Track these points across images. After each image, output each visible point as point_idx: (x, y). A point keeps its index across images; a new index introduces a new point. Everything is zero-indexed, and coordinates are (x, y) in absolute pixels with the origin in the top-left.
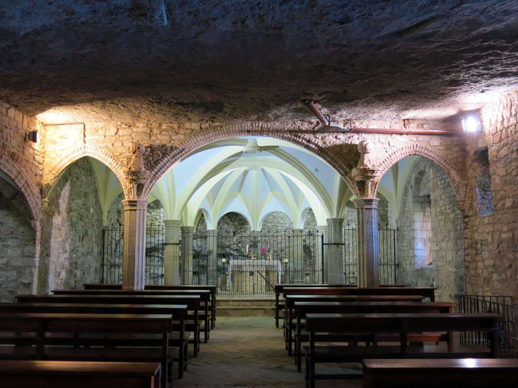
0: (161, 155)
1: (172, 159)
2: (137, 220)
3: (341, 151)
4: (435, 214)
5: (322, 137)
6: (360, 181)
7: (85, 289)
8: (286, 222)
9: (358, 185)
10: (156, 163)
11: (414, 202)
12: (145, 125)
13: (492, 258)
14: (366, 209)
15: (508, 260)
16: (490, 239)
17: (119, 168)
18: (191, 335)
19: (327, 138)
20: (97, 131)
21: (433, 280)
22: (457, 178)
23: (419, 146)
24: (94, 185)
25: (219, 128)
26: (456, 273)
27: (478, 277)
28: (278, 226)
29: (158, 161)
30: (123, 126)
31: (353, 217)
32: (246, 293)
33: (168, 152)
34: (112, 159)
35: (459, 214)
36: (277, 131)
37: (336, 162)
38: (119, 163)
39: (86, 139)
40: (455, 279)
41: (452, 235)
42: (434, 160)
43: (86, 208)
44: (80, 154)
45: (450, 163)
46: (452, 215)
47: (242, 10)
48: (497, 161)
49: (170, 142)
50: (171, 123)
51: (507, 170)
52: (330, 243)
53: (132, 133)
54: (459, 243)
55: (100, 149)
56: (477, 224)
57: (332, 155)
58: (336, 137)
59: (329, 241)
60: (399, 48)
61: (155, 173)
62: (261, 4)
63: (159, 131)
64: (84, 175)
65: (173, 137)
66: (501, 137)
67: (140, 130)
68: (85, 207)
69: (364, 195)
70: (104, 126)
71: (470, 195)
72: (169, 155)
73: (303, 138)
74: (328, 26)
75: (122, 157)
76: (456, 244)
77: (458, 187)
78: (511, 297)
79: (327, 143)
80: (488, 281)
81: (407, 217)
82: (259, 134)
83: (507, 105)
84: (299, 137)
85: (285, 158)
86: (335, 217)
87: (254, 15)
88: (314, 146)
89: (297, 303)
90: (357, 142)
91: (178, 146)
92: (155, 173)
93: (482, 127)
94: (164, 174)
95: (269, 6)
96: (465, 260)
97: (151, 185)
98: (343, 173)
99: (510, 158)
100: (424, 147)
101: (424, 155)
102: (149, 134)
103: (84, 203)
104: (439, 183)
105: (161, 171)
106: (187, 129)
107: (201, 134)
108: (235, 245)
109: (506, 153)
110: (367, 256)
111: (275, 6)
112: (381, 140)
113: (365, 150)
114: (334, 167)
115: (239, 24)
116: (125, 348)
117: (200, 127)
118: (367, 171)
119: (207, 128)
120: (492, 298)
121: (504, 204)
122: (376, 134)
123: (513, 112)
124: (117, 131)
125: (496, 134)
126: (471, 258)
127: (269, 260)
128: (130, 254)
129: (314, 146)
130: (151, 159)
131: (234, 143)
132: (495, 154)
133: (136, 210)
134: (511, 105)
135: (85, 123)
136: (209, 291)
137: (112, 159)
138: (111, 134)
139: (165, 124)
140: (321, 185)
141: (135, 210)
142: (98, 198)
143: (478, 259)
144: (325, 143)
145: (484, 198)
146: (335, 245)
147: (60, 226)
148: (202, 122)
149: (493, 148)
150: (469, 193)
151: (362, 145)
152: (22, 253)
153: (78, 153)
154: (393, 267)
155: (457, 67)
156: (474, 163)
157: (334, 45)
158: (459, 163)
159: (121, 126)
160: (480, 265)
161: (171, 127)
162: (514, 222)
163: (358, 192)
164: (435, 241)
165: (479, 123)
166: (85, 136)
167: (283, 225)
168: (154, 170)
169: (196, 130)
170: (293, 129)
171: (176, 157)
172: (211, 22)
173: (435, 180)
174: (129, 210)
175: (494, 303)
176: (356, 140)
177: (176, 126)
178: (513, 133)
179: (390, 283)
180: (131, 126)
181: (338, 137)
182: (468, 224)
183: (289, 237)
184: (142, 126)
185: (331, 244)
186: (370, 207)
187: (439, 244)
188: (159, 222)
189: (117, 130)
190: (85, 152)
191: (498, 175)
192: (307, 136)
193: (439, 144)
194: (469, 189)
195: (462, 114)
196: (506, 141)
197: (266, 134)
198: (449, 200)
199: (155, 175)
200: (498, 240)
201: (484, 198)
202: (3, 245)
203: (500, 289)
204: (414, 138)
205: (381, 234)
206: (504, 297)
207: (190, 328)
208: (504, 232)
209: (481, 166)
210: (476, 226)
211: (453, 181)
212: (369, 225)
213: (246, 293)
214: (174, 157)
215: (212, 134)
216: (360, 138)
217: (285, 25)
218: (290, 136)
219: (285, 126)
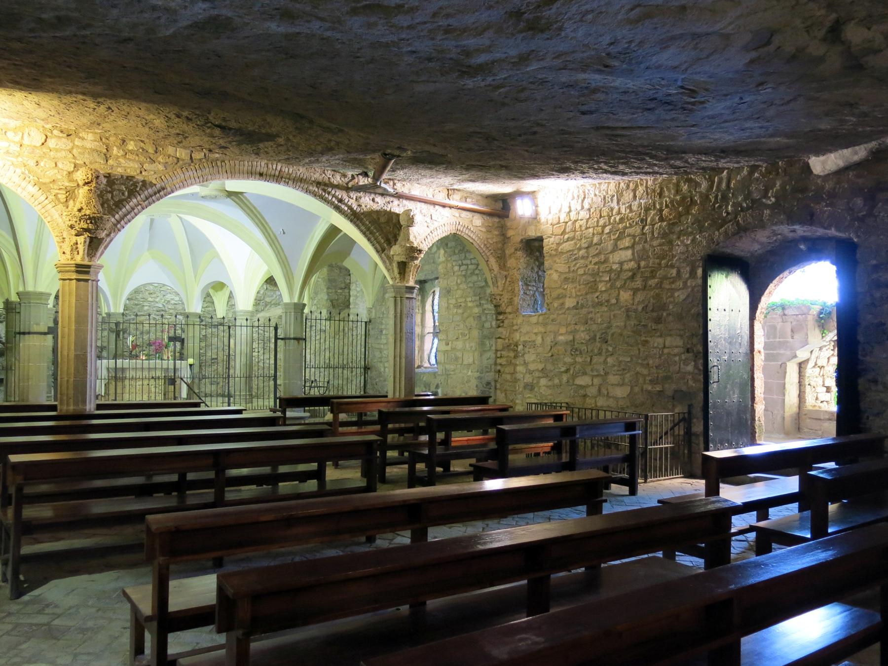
0: (126, 193)
1: (144, 201)
3: (379, 219)
4: (446, 305)
5: (357, 197)
6: (402, 262)
8: (157, 300)
10: (119, 204)
13: (540, 362)
15: (565, 363)
16: (539, 340)
19: (363, 198)
20: (6, 132)
21: (437, 387)
22: (495, 267)
23: (461, 224)
25: (219, 163)
26: (479, 378)
27: (516, 382)
28: (143, 306)
30: (56, 132)
31: (273, 298)
32: (265, 408)
33: (138, 189)
34: (37, 188)
36: (301, 180)
38: (51, 197)
40: (477, 386)
41: (475, 333)
42: (474, 243)
45: (490, 248)
46: (476, 309)
48: (556, 255)
50: (142, 141)
51: (569, 267)
52: (288, 337)
53: (73, 148)
55: (12, 167)
56: (519, 323)
58: (373, 200)
59: (286, 334)
61: (115, 222)
65: (146, 166)
66: (565, 229)
67: (89, 145)
69: (404, 280)
71: (510, 288)
72: (140, 195)
73: (334, 196)
75: (55, 187)
76: (482, 344)
77: (496, 278)
79: (363, 206)
80: (530, 387)
82: (275, 180)
83: (578, 196)
84: (329, 193)
86: (296, 300)
88: (346, 209)
90: (397, 210)
91: (154, 182)
92: (115, 222)
93: (537, 214)
94: (129, 224)
96: (496, 364)
99: (576, 254)
100: (466, 226)
101: (465, 236)
102: (105, 155)
104: (456, 268)
105: (126, 219)
106: (169, 156)
107: (191, 167)
109: (571, 249)
110: (406, 358)
112: (423, 212)
113: (411, 221)
116: (206, 489)
117: (191, 156)
118: (414, 250)
119: (200, 160)
121: (563, 304)
122: (418, 203)
123: (586, 206)
124: (46, 141)
125: (557, 224)
126: (507, 361)
127: (168, 360)
128: (78, 353)
129: (346, 209)
130: (110, 198)
132: (554, 246)
133: (89, 280)
134: (584, 198)
138: (33, 144)
139: (132, 142)
140: (285, 255)
141: (87, 280)
143: (518, 363)
144: (360, 206)
145: (526, 294)
146: (295, 341)
149: (552, 240)
150: (508, 286)
151: (409, 215)
156: (518, 253)
158: (498, 249)
159: (52, 132)
160: (520, 369)
161: (143, 149)
162: (576, 324)
163: (398, 276)
164: (443, 340)
165: (534, 208)
167: (153, 304)
168: (118, 213)
169: (183, 160)
170: (321, 181)
171: (150, 200)
173: (449, 265)
176: (397, 207)
178: (583, 228)
181: (376, 200)
182: (503, 322)
184: (93, 139)
185: (290, 339)
186: (411, 296)
187: (450, 343)
189: (45, 137)
191: (556, 271)
192: (340, 193)
193: (481, 224)
194: (509, 282)
195: (518, 194)
196: (572, 235)
197: (285, 181)
198: (474, 292)
199: (115, 225)
201: (526, 294)
203: (551, 395)
204: (456, 213)
205: (332, 325)
208: (562, 334)
209: (525, 256)
210: (517, 325)
211: (490, 270)
212: (409, 319)
213: (254, 408)
214: (147, 198)
216: (401, 205)
218: (317, 190)
219: (312, 174)
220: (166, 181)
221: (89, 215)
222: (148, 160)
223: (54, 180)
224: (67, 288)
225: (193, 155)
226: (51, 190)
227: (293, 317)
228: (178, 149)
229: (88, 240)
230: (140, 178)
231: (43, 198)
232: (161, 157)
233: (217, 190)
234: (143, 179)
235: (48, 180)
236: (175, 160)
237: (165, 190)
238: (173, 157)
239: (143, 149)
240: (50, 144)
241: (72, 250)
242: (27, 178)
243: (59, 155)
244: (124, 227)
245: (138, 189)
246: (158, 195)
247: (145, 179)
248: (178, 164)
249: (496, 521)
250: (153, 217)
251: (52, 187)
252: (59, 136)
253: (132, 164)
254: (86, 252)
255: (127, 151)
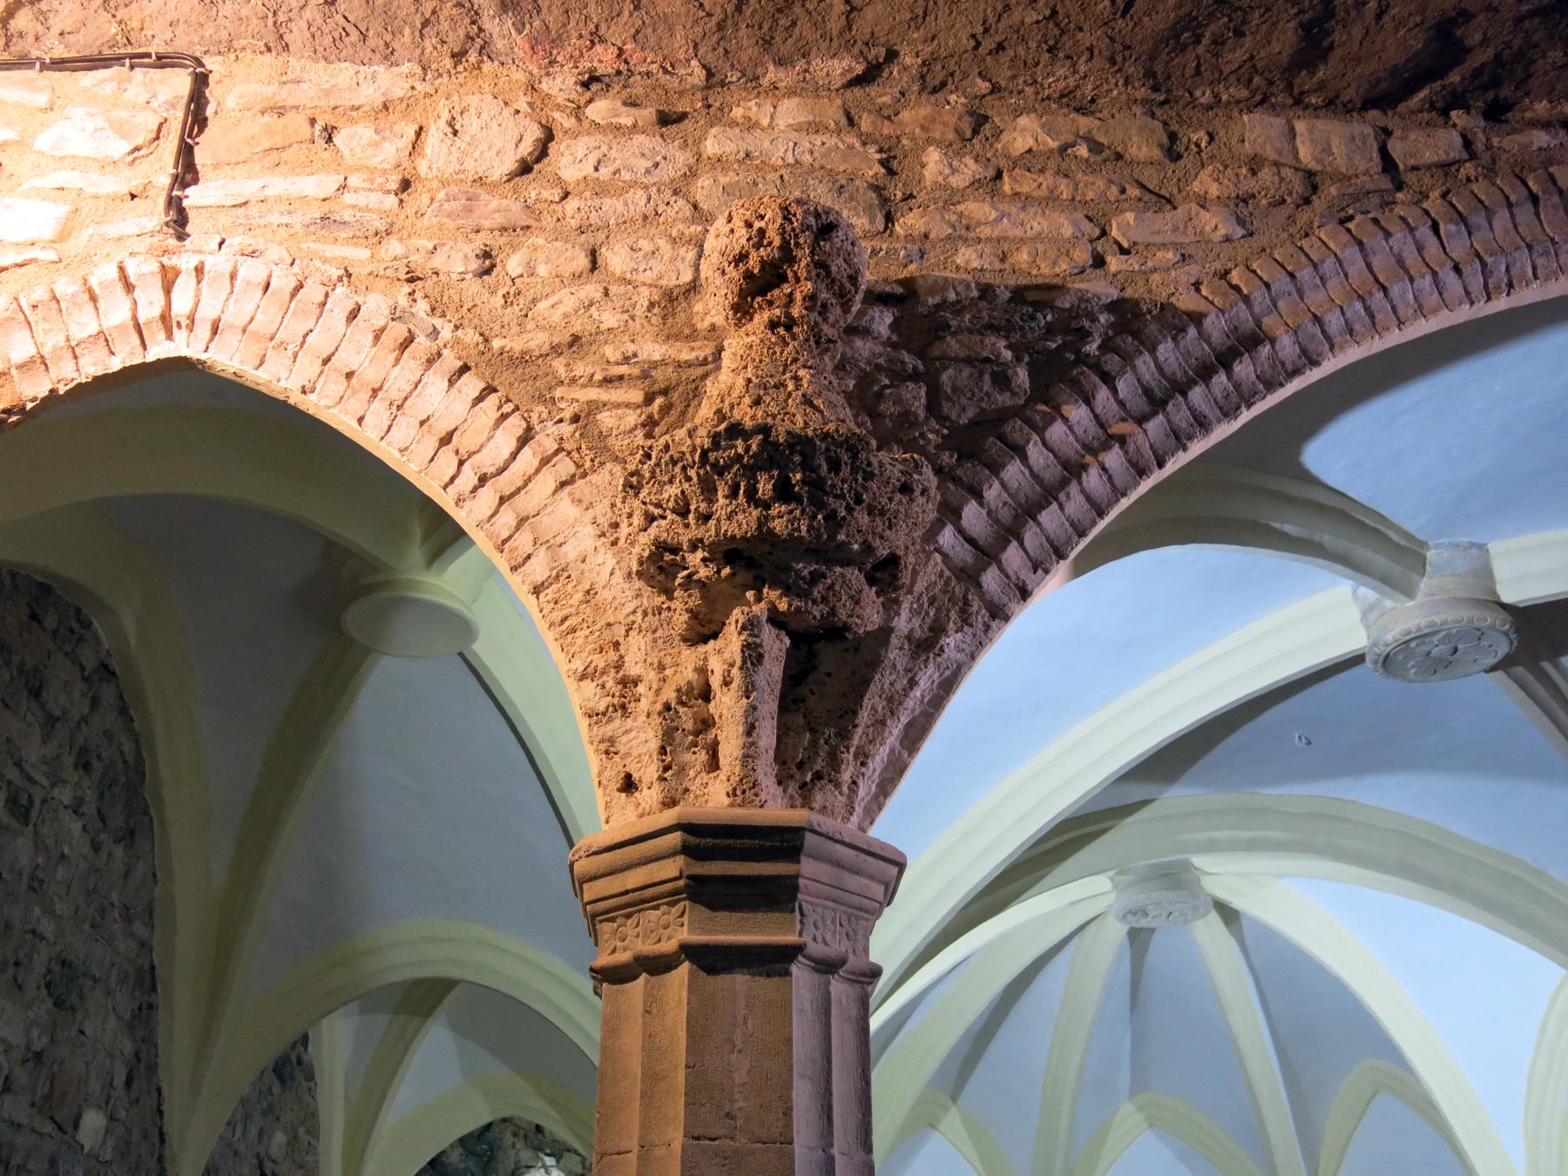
0: (1022, 376)
1: (1141, 420)
2: (802, 1095)
12: (832, 112)
17: (546, 482)
24: (139, 927)
29: (992, 422)
33: (1092, 348)
34: (471, 385)
39: (193, 197)
43: (48, 1097)
44: (104, 339)
49: (1099, 262)
53: (691, 174)
63: (970, 169)
64: (76, 808)
68: (42, 1089)
70: (408, 103)
72: (1109, 380)
75: (581, 369)
91: (1186, 301)
97: (927, 678)
103: (40, 1043)
106: (1255, 165)
107: (1400, 210)
124: (542, 152)
130: (919, 406)
133: (790, 953)
135: (211, 63)
137: (471, 385)
141: (775, 960)
142: (150, 1041)
148: (1391, 121)
153: (84, 325)
161: (1096, 147)
166: (187, 173)
168: (978, 495)
171: (1179, 413)
174: (690, 952)
177: (1142, 146)
180: (682, 117)
189: (534, 133)
190: (165, 319)
199: (969, 576)
214: (1157, 404)
215: (1502, 218)
220: (1259, 296)
221: (765, 430)
222: (1134, 192)
223: (576, 339)
224: (632, 1041)
225: (1396, 148)
226: (558, 393)
228: (1300, 126)
229: (775, 645)
230: (1101, 288)
231: (505, 441)
232: (1205, 174)
233: (1457, 601)
234: (1114, 294)
235: (537, 341)
236: (1298, 185)
237: (1265, 350)
238: (1276, 164)
239: (1096, 147)
240: (565, 160)
241: (668, 737)
242: (421, 340)
243: (612, 206)
244: (1024, 594)
245: (1092, 348)
247: (1129, 293)
248: (1318, 203)
250: (1144, 923)
251: (562, 372)
252: (618, 128)
253: (1037, 224)
254: (767, 737)
255: (1002, 163)
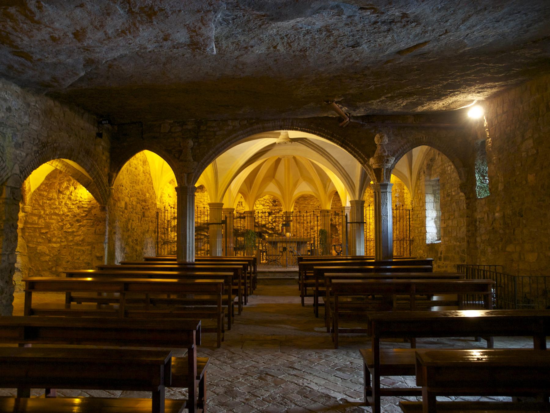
6: (377, 168)
7: (145, 261)
9: (375, 172)
11: (426, 185)
14: (382, 192)
18: (236, 299)
35: (463, 196)
37: (356, 152)
47: (274, 40)
54: (462, 220)
57: (352, 146)
60: (402, 63)
62: (289, 36)
74: (343, 49)
78: (502, 266)
81: (420, 198)
85: (313, 148)
86: (357, 199)
87: (283, 43)
89: (334, 281)
95: (295, 36)
98: (362, 162)
108: (270, 224)
111: (300, 37)
114: (354, 156)
115: (272, 49)
120: (491, 267)
131: (270, 136)
136: (247, 263)
147: (123, 209)
152: (95, 232)
154: (408, 242)
155: (452, 75)
157: (349, 61)
160: (478, 239)
163: (375, 178)
172: (250, 48)
175: (487, 271)
179: (405, 256)
183: (317, 217)
185: (355, 223)
186: (385, 191)
188: (203, 204)
200: (492, 218)
202: (80, 225)
206: (495, 266)
207: (236, 292)
217: (308, 48)
227: (355, 209)
246: (223, 147)
249: (344, 352)
